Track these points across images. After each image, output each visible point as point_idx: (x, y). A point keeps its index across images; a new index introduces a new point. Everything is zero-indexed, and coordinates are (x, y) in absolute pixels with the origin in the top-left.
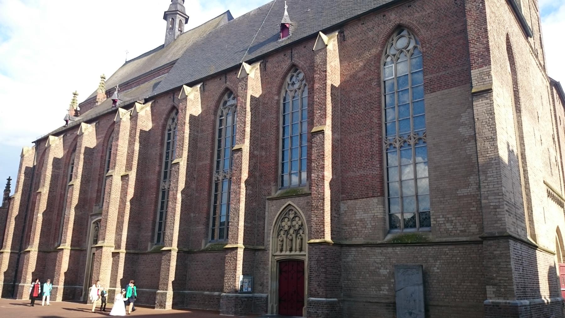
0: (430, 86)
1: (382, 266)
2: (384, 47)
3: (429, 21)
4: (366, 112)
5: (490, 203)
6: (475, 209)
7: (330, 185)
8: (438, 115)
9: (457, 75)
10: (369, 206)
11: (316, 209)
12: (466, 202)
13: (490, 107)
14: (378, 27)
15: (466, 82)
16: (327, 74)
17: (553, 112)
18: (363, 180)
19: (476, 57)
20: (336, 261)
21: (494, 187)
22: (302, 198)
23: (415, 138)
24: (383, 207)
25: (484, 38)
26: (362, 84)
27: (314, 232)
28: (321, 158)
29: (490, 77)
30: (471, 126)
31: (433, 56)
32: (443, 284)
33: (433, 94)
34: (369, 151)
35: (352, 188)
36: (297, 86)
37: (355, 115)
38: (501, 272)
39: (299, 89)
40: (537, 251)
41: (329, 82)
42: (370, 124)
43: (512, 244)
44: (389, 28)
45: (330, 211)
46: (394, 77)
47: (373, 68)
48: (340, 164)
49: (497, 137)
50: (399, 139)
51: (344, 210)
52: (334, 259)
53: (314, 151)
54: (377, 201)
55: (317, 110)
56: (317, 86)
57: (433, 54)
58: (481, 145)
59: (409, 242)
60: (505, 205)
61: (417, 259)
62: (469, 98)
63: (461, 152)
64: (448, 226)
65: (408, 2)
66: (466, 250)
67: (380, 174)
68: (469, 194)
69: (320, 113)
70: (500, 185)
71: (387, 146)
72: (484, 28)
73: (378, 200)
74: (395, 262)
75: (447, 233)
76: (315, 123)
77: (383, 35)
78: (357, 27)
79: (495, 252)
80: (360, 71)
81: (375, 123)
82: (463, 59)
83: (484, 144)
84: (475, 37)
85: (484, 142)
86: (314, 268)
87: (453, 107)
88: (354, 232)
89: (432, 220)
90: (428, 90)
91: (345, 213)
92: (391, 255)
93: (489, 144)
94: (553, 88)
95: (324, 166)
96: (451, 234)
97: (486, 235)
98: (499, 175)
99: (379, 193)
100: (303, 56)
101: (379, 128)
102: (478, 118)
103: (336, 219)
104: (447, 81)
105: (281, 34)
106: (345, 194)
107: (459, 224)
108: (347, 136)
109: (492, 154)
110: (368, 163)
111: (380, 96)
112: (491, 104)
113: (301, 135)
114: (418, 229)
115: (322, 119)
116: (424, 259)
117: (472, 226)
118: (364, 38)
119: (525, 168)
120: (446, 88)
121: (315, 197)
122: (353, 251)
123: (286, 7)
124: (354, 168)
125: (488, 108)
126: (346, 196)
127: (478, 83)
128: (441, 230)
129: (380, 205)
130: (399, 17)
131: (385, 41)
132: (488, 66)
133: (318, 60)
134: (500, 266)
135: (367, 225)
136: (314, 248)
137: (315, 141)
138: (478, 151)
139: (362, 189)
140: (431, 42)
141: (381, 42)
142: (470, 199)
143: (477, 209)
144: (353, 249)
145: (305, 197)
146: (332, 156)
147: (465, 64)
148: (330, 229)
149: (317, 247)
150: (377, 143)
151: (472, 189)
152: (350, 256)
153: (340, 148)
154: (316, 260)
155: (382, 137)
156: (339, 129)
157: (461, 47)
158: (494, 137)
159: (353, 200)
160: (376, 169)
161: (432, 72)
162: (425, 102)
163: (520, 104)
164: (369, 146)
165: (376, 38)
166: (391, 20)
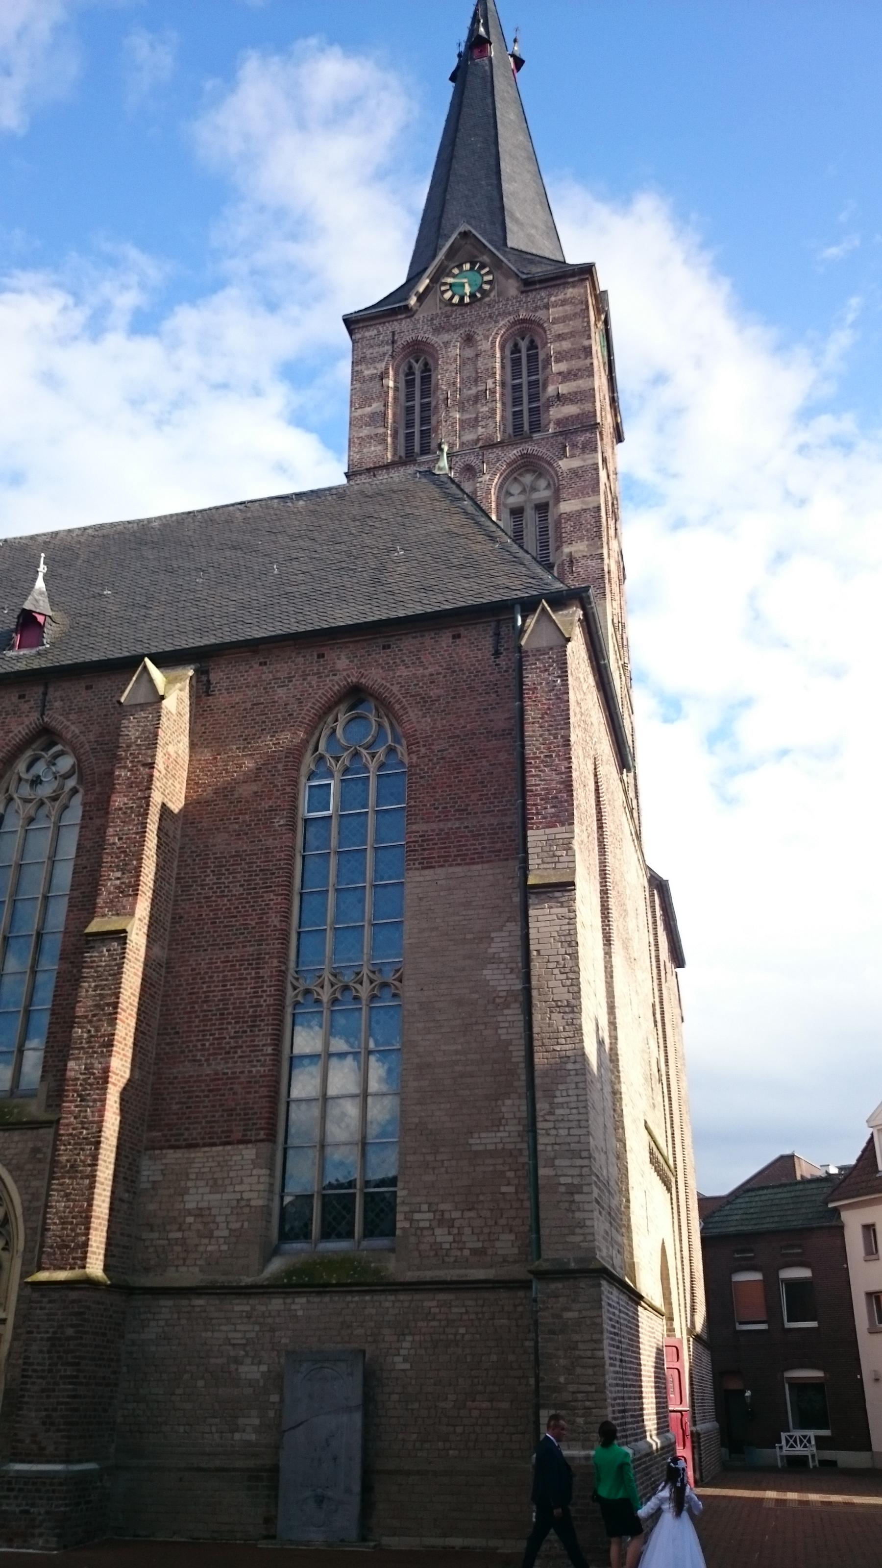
0: (420, 852)
1: (247, 1355)
2: (312, 734)
3: (431, 694)
4: (250, 894)
5: (560, 1176)
6: (511, 1189)
7: (122, 1099)
8: (437, 928)
9: (488, 834)
10: (228, 1172)
11: (68, 1172)
12: (491, 1168)
13: (567, 927)
14: (304, 680)
15: (507, 855)
16: (156, 773)
17: (653, 948)
18: (220, 1089)
19: (541, 800)
20: (108, 1341)
21: (569, 1135)
22: (16, 1136)
23: (371, 982)
24: (270, 1175)
25: (563, 760)
26: (247, 816)
27: (51, 1247)
28: (104, 1015)
29: (570, 853)
30: (514, 965)
31: (435, 780)
32: (416, 1405)
33: (427, 872)
34: (248, 1005)
35: (184, 1113)
36: (46, 790)
37: (218, 897)
38: (579, 1370)
39: (54, 799)
40: (640, 1309)
41: (157, 798)
42: (257, 930)
43: (606, 1293)
44: (330, 688)
45: (110, 1183)
46: (331, 812)
47: (279, 781)
48: (156, 1037)
49: (580, 1005)
50: (332, 978)
51: (151, 1179)
52: (104, 1334)
53: (87, 992)
54: (254, 1157)
55: (113, 871)
56: (118, 801)
57: (436, 773)
58: (543, 1019)
59: (334, 1282)
60: (593, 1186)
61: (349, 1331)
62: (513, 895)
63: (485, 1033)
64: (442, 1236)
65: (384, 637)
66: (483, 1306)
67: (273, 1076)
68: (500, 1146)
69: (118, 879)
70: (584, 1131)
71: (296, 996)
72: (562, 737)
73: (257, 1153)
74: (287, 1341)
75: (436, 1255)
76: (101, 908)
77: (314, 703)
78: (248, 666)
79: (568, 1315)
80: (243, 782)
81: (272, 928)
82: (504, 799)
83: (550, 1019)
84: (542, 752)
85: (551, 1012)
86: (38, 1364)
87: (473, 912)
88: (172, 1251)
89: (400, 1217)
90: (415, 860)
91: (153, 1188)
92: (278, 1320)
93: (563, 1018)
94: (655, 892)
95: (113, 1040)
96: (446, 1259)
97: (546, 1266)
98: (583, 1104)
99: (262, 1132)
100: (80, 711)
101: (282, 944)
102: (538, 951)
103: (125, 1206)
104: (464, 845)
105: (18, 639)
106: (160, 1131)
107: (470, 1232)
108: (187, 954)
109: (567, 1047)
110: (240, 1041)
111: (292, 857)
112: (571, 919)
113: (39, 935)
114: (359, 1243)
115: (124, 896)
116: (369, 1333)
117: (502, 1237)
118: (262, 700)
119: (616, 1087)
120: (459, 862)
121: (71, 1134)
122: (163, 1310)
123: (42, 569)
124: (197, 1050)
125: (564, 928)
126: (164, 1135)
127: (543, 863)
128: (422, 1247)
129: (261, 1168)
130: (358, 668)
131: (316, 718)
132: (567, 827)
133: (132, 729)
134: (577, 1353)
135: (217, 1228)
136: (46, 1300)
137: (93, 962)
138: (535, 1036)
139: (214, 1116)
140: (433, 744)
141: (308, 718)
142: (500, 1161)
143: (516, 1193)
144: (167, 1303)
145: (29, 1132)
146: (139, 1009)
147: (508, 812)
148: (104, 1240)
149: (55, 1296)
150: (273, 983)
151: (506, 1134)
152: (153, 1324)
153: (162, 989)
154: (49, 1339)
155: (287, 969)
156: (167, 933)
157: (500, 769)
158: (573, 1002)
159: (183, 1150)
160: (262, 1058)
161: (429, 818)
162: (406, 891)
163: (609, 925)
164: (249, 990)
165: (294, 706)
166: (338, 671)
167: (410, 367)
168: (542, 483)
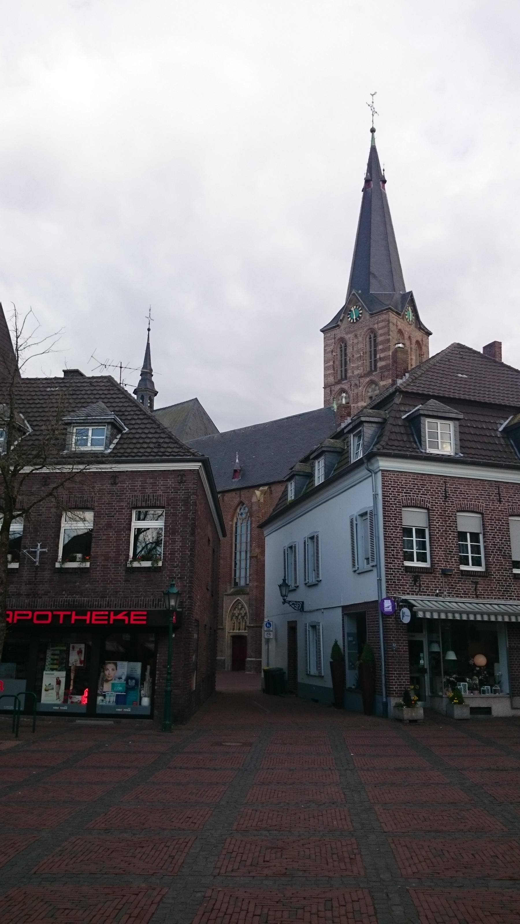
167: (341, 345)
168: (377, 388)
